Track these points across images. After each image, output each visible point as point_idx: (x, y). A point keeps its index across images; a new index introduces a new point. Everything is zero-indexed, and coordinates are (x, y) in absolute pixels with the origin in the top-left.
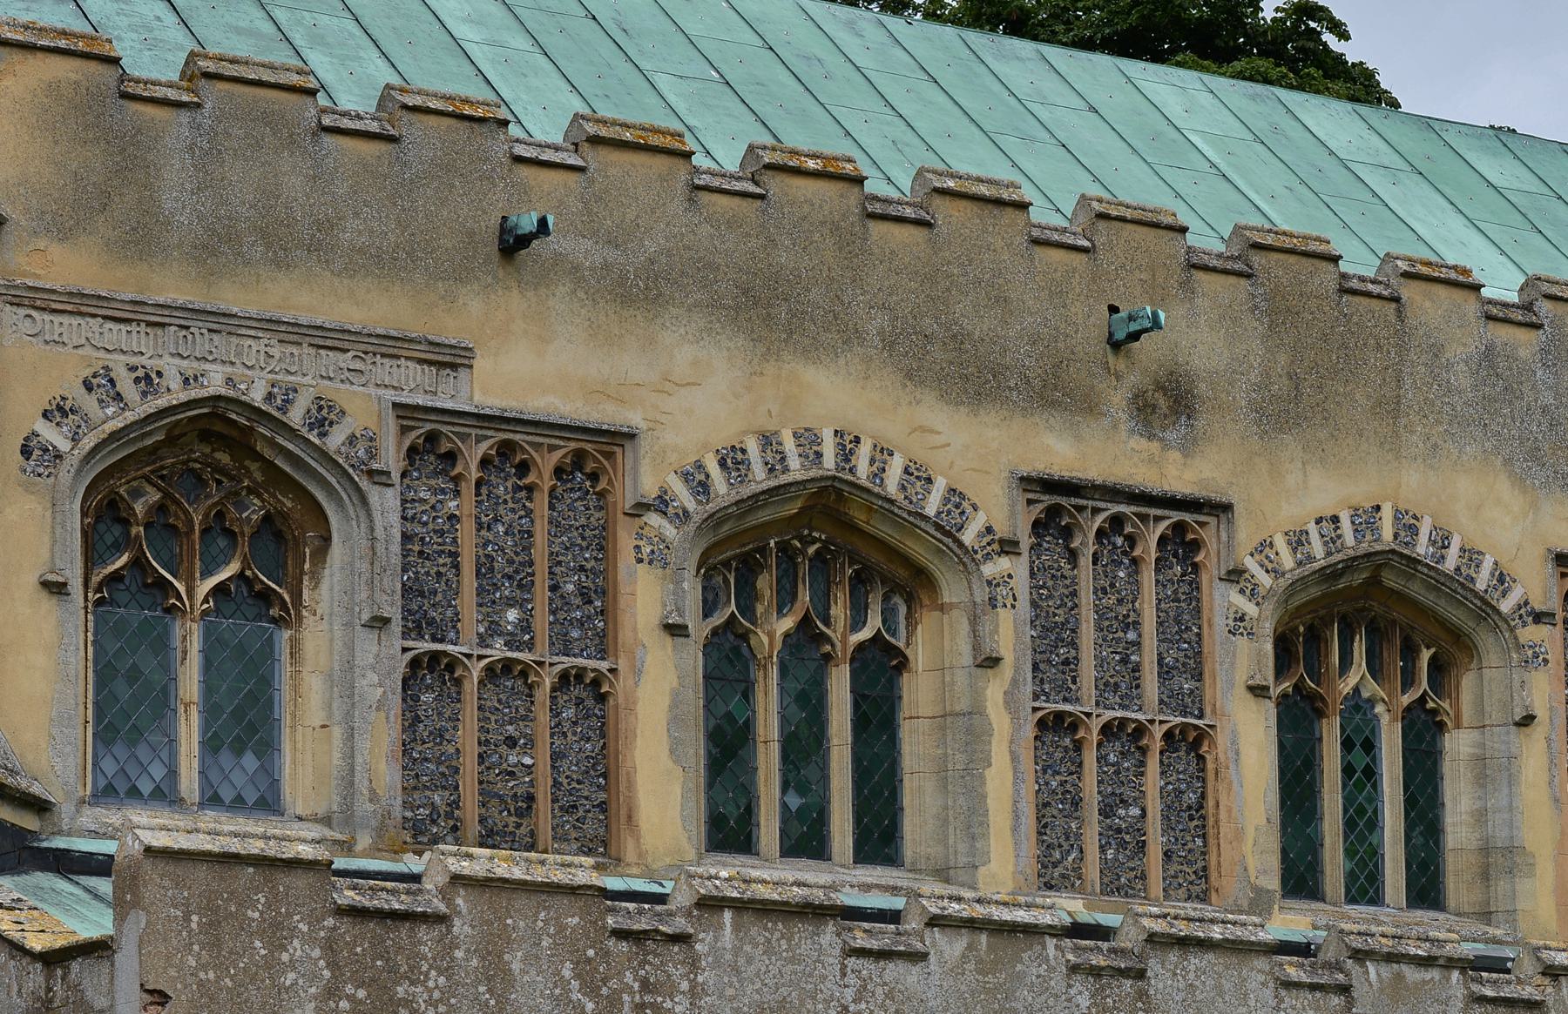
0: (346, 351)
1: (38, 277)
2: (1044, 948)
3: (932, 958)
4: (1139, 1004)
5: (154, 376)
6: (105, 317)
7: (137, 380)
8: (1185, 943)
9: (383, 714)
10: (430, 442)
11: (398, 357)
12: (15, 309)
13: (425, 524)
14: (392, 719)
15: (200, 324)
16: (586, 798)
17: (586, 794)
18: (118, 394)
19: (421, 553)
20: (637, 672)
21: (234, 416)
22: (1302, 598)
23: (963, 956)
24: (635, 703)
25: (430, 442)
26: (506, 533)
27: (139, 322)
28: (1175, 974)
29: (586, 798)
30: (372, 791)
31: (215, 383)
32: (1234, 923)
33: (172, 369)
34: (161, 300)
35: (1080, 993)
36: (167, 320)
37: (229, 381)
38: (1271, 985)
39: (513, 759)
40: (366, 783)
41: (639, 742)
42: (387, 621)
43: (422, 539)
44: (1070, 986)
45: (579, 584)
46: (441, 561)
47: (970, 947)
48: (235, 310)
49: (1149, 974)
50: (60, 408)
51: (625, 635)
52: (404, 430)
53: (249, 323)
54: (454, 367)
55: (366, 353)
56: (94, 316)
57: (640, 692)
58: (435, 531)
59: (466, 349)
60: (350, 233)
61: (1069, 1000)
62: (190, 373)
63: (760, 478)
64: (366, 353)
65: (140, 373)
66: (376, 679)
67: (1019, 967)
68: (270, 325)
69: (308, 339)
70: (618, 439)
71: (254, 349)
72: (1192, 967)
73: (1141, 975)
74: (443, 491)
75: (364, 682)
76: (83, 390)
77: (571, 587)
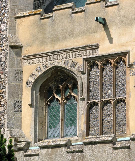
0: (77, 51)
1: (27, 54)
2: (62, 149)
3: (40, 154)
4: (82, 157)
5: (46, 65)
6: (39, 57)
7: (44, 67)
8: (92, 143)
9: (83, 115)
10: (91, 63)
11: (86, 50)
12: (25, 60)
13: (94, 79)
14: (85, 116)
15: (53, 54)
16: (123, 123)
17: (123, 122)
18: (41, 70)
19: (93, 84)
20: (129, 97)
21: (59, 68)
22: (71, 76)
23: (46, 153)
24: (129, 103)
25: (91, 63)
26: (108, 77)
27: (44, 57)
28: (90, 150)
29: (123, 123)
30: (81, 130)
31: (56, 63)
32: (21, 144)
33: (49, 63)
34: (46, 52)
35: (69, 157)
36: (48, 55)
37: (58, 62)
38: (111, 149)
39: (109, 119)
40: (80, 128)
41: (130, 111)
42: (84, 99)
43: (93, 82)
44: (67, 156)
45: (122, 83)
46: (97, 85)
47: (47, 151)
48: (57, 50)
49: (84, 150)
50: (32, 75)
51: (128, 91)
52: (88, 63)
53: (60, 52)
54: (97, 49)
55: (81, 51)
56: (37, 58)
57: (130, 101)
58: (96, 79)
59: (97, 45)
60: (77, 30)
61: (67, 158)
62: (52, 63)
63: (43, 70)
64: (81, 51)
65: (44, 65)
66: (82, 109)
67: (57, 153)
68: (64, 51)
69: (71, 51)
70: (125, 54)
71: (62, 56)
72: (94, 148)
73: (82, 151)
74: (97, 72)
75: (80, 110)
76: (36, 71)
77: (120, 84)
